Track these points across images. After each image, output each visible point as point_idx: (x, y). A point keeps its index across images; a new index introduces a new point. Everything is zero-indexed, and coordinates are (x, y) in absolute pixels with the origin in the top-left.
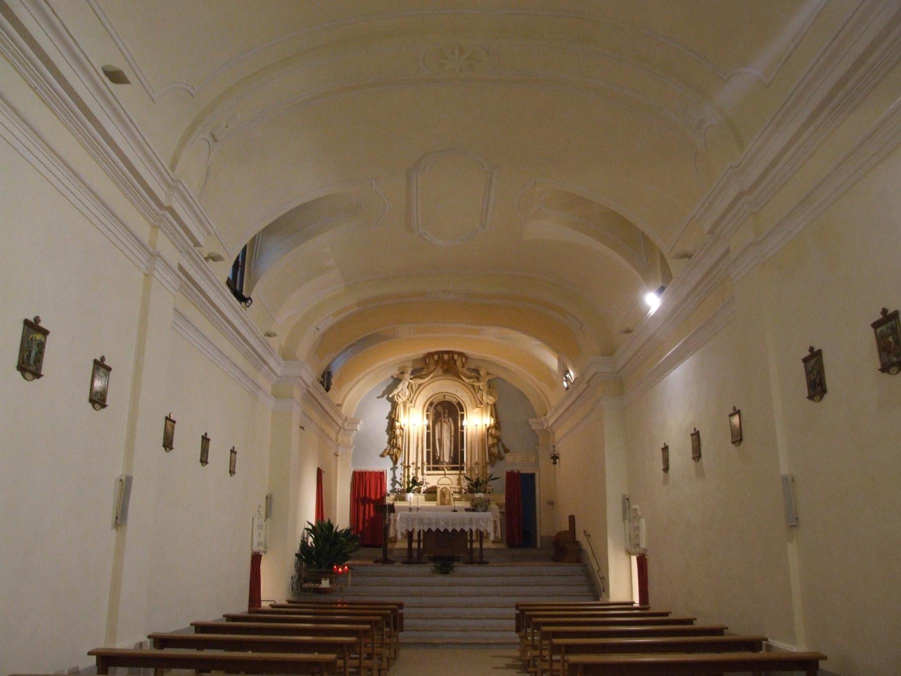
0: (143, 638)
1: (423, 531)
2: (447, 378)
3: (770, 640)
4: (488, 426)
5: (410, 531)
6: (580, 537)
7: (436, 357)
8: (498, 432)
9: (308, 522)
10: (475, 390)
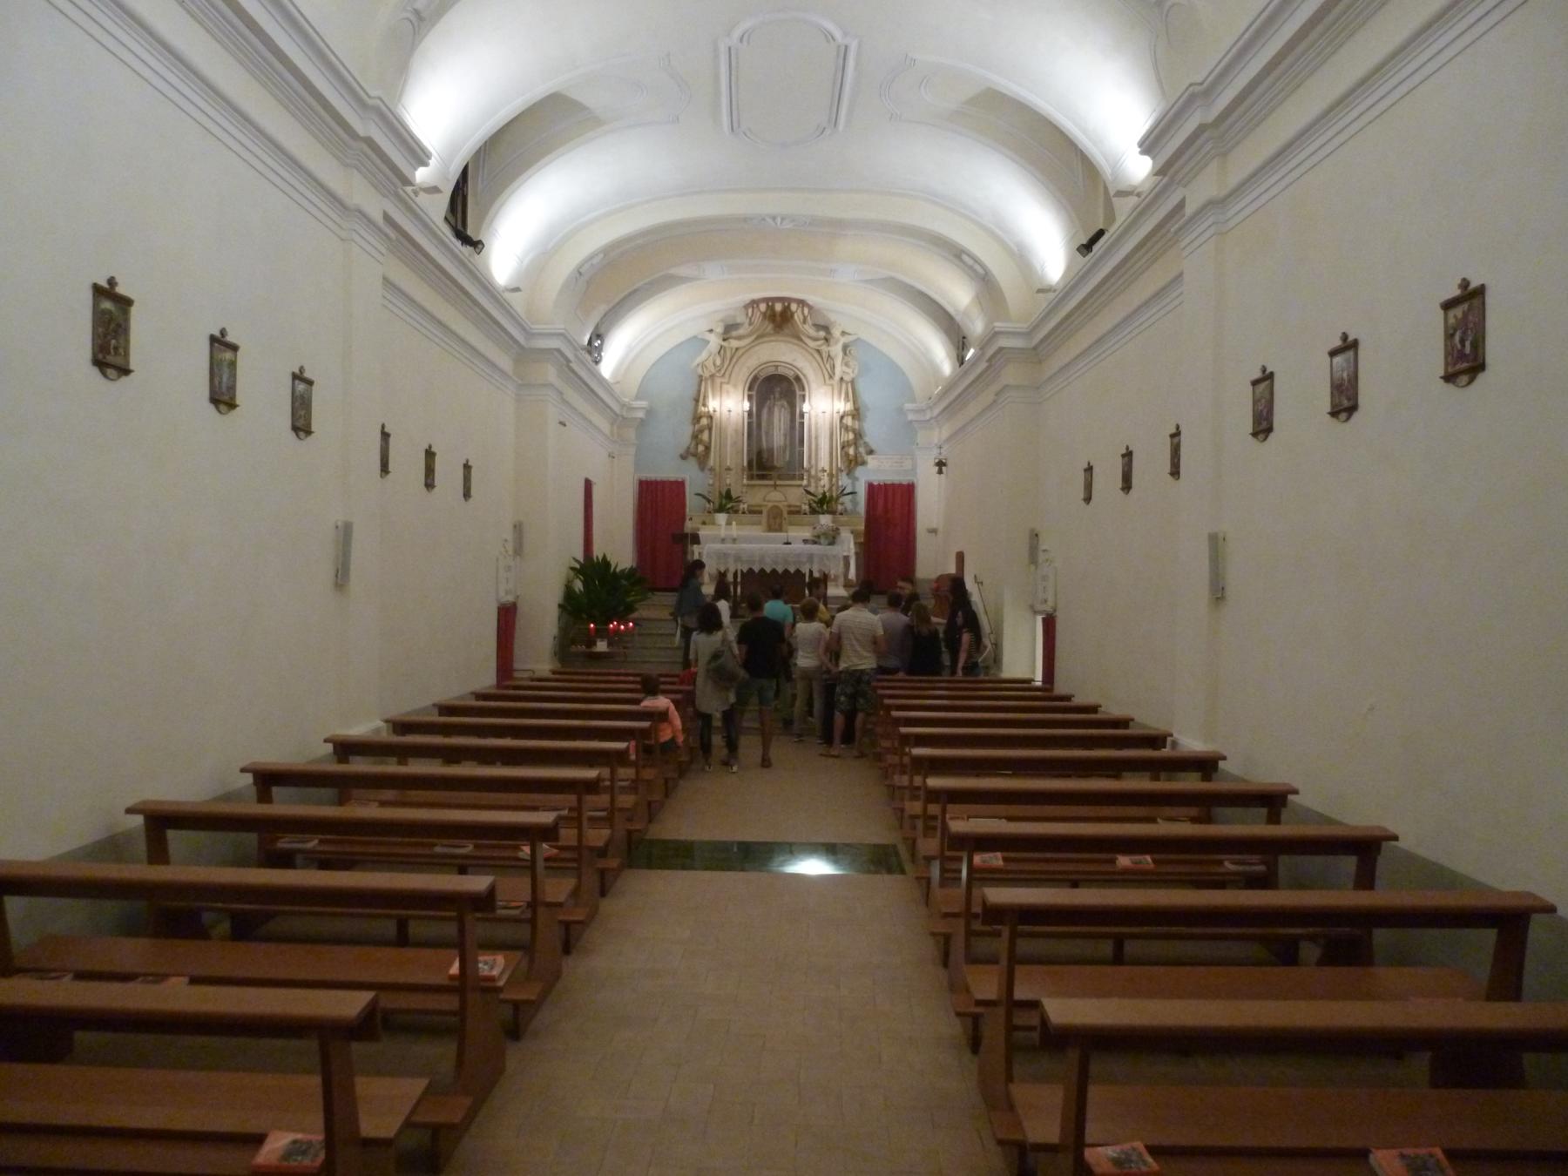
0: (379, 723)
1: (742, 571)
2: (780, 338)
3: (1175, 735)
4: (841, 413)
5: (722, 571)
6: (970, 585)
7: (763, 307)
8: (857, 422)
9: (574, 559)
10: (822, 358)
